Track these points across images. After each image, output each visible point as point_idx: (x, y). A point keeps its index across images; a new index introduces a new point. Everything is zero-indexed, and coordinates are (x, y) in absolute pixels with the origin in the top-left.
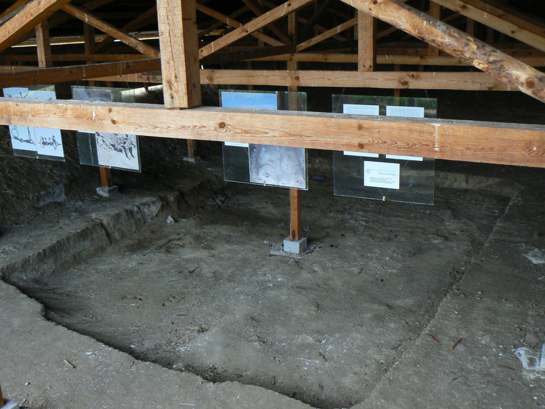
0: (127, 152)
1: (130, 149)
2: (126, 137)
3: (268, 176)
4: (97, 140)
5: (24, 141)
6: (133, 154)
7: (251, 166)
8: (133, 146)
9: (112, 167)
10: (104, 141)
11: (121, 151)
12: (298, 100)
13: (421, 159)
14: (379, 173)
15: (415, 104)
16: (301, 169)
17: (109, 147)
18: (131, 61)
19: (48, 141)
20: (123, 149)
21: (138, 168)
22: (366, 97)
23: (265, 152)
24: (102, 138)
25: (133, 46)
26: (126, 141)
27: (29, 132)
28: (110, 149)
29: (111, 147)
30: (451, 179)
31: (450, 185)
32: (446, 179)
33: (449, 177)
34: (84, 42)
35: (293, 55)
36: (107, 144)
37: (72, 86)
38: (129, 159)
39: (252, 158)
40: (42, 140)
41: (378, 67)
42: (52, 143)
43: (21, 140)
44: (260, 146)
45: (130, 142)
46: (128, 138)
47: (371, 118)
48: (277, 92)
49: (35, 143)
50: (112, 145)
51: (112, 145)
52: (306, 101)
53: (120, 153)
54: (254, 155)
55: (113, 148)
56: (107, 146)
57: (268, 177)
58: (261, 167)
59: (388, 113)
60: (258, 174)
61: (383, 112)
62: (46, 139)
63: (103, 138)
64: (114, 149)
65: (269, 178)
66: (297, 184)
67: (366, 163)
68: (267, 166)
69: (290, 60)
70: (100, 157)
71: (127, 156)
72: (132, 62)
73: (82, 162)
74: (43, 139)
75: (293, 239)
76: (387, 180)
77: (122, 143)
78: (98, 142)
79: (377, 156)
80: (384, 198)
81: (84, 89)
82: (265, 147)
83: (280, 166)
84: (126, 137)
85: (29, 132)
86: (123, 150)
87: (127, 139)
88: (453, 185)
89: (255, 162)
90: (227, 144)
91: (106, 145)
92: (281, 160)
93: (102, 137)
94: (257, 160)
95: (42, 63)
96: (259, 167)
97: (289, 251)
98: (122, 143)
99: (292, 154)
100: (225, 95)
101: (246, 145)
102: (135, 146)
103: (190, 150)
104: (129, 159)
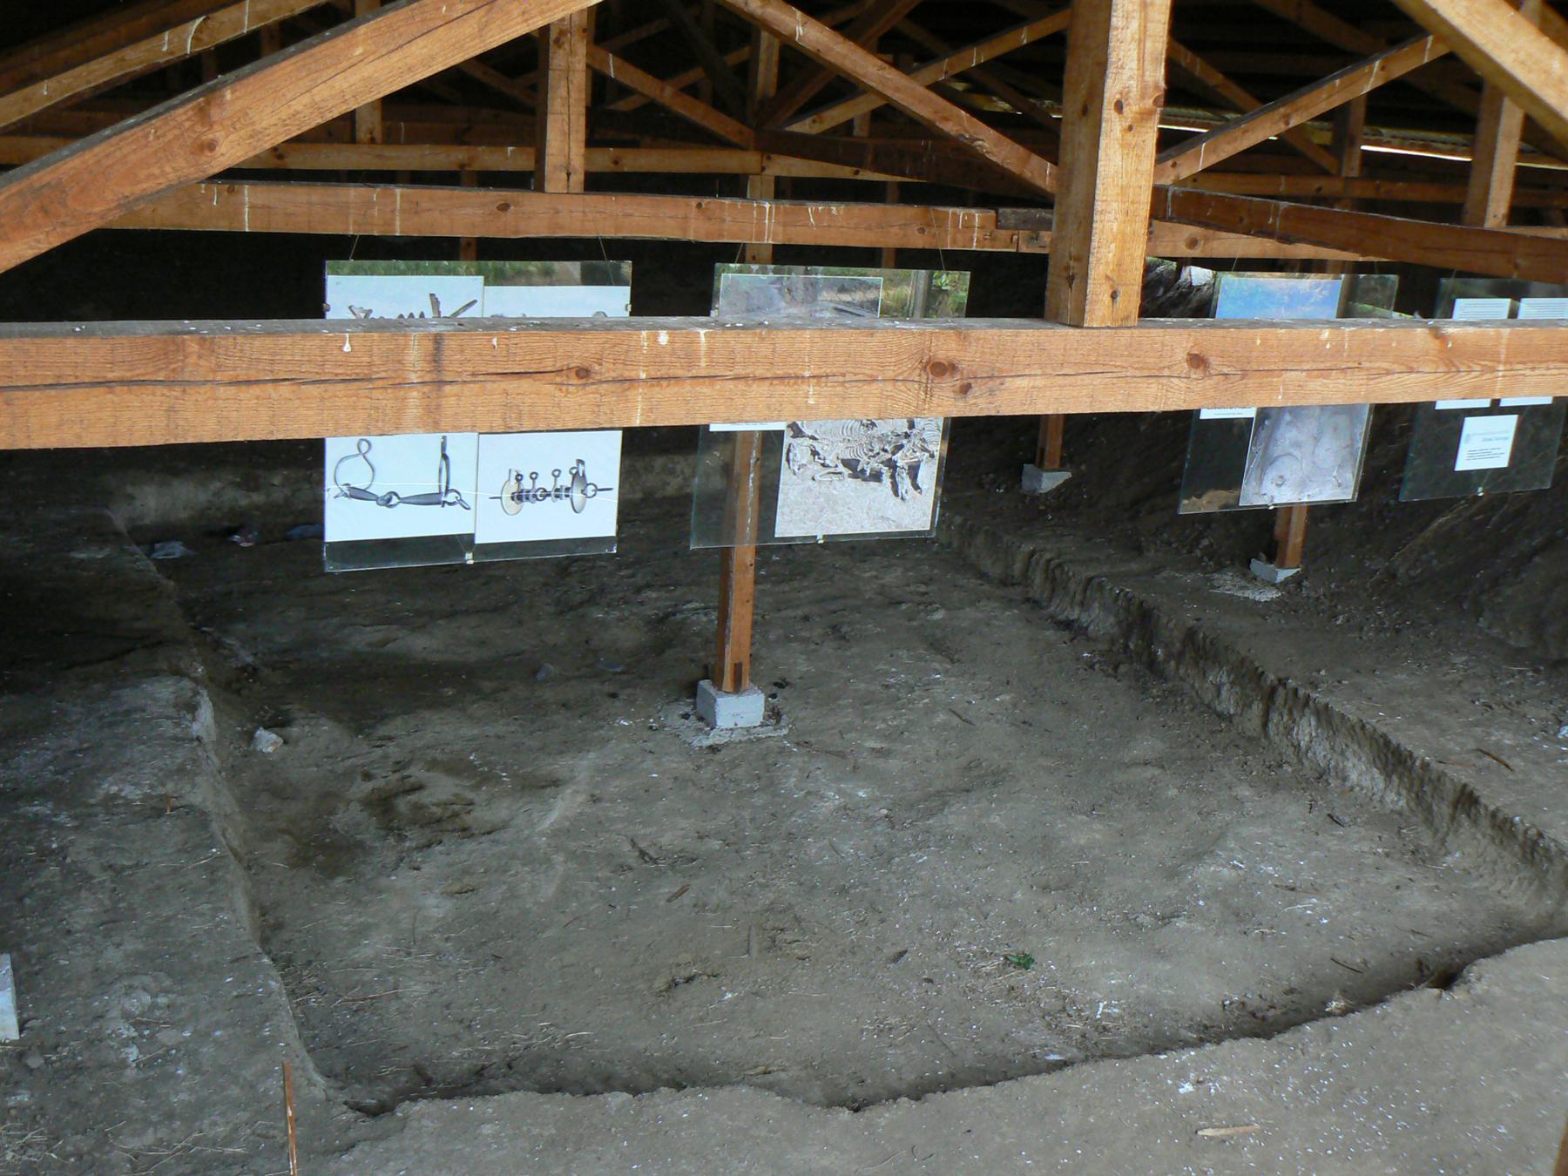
0: (898, 479)
1: (913, 471)
2: (907, 430)
3: (1281, 482)
4: (789, 451)
5: (403, 500)
6: (919, 481)
7: (1250, 464)
8: (927, 454)
9: (824, 536)
10: (815, 453)
11: (877, 477)
12: (804, 284)
13: (1548, 400)
14: (1485, 440)
15: (1097, 289)
16: (1353, 454)
17: (832, 470)
18: (899, 179)
19: (546, 482)
20: (885, 469)
21: (819, 529)
22: (533, 266)
23: (1289, 423)
24: (811, 442)
25: (962, 136)
26: (905, 442)
27: (445, 457)
28: (835, 478)
29: (841, 468)
30: (683, 472)
31: (681, 488)
32: (672, 472)
33: (679, 468)
34: (1469, 160)
35: (769, 158)
36: (827, 462)
37: (718, 265)
38: (902, 499)
39: (1255, 445)
40: (513, 481)
41: (596, 183)
42: (568, 489)
43: (387, 502)
44: (1281, 410)
45: (919, 444)
46: (914, 431)
47: (600, 325)
48: (1343, 276)
49: (470, 502)
50: (846, 463)
51: (846, 463)
52: (1394, 300)
53: (873, 484)
54: (1263, 434)
55: (846, 471)
56: (828, 466)
57: (1280, 485)
58: (1272, 463)
59: (1521, 316)
60: (1261, 483)
61: (1513, 314)
62: (534, 476)
63: (815, 444)
64: (850, 476)
65: (1283, 488)
66: (1338, 490)
67: (1470, 423)
68: (1285, 459)
69: (759, 170)
70: (786, 510)
71: (896, 493)
72: (901, 184)
73: (699, 540)
74: (519, 478)
75: (737, 688)
76: (1494, 452)
77: (885, 451)
78: (788, 460)
79: (1486, 403)
80: (1480, 489)
81: (771, 275)
82: (1290, 412)
83: (1313, 453)
84: (907, 430)
85: (445, 457)
86: (887, 480)
87: (907, 436)
88: (688, 486)
89: (1260, 453)
90: (1206, 415)
91: (823, 465)
92: (1317, 439)
93: (813, 438)
94: (1266, 448)
95: (569, 174)
96: (1267, 462)
97: (732, 726)
98: (885, 451)
99: (1342, 421)
100: (729, 278)
101: (1251, 413)
102: (932, 456)
103: (1053, 444)
104: (902, 499)
